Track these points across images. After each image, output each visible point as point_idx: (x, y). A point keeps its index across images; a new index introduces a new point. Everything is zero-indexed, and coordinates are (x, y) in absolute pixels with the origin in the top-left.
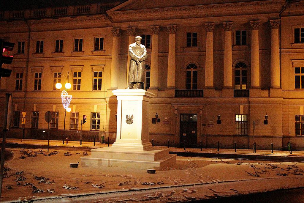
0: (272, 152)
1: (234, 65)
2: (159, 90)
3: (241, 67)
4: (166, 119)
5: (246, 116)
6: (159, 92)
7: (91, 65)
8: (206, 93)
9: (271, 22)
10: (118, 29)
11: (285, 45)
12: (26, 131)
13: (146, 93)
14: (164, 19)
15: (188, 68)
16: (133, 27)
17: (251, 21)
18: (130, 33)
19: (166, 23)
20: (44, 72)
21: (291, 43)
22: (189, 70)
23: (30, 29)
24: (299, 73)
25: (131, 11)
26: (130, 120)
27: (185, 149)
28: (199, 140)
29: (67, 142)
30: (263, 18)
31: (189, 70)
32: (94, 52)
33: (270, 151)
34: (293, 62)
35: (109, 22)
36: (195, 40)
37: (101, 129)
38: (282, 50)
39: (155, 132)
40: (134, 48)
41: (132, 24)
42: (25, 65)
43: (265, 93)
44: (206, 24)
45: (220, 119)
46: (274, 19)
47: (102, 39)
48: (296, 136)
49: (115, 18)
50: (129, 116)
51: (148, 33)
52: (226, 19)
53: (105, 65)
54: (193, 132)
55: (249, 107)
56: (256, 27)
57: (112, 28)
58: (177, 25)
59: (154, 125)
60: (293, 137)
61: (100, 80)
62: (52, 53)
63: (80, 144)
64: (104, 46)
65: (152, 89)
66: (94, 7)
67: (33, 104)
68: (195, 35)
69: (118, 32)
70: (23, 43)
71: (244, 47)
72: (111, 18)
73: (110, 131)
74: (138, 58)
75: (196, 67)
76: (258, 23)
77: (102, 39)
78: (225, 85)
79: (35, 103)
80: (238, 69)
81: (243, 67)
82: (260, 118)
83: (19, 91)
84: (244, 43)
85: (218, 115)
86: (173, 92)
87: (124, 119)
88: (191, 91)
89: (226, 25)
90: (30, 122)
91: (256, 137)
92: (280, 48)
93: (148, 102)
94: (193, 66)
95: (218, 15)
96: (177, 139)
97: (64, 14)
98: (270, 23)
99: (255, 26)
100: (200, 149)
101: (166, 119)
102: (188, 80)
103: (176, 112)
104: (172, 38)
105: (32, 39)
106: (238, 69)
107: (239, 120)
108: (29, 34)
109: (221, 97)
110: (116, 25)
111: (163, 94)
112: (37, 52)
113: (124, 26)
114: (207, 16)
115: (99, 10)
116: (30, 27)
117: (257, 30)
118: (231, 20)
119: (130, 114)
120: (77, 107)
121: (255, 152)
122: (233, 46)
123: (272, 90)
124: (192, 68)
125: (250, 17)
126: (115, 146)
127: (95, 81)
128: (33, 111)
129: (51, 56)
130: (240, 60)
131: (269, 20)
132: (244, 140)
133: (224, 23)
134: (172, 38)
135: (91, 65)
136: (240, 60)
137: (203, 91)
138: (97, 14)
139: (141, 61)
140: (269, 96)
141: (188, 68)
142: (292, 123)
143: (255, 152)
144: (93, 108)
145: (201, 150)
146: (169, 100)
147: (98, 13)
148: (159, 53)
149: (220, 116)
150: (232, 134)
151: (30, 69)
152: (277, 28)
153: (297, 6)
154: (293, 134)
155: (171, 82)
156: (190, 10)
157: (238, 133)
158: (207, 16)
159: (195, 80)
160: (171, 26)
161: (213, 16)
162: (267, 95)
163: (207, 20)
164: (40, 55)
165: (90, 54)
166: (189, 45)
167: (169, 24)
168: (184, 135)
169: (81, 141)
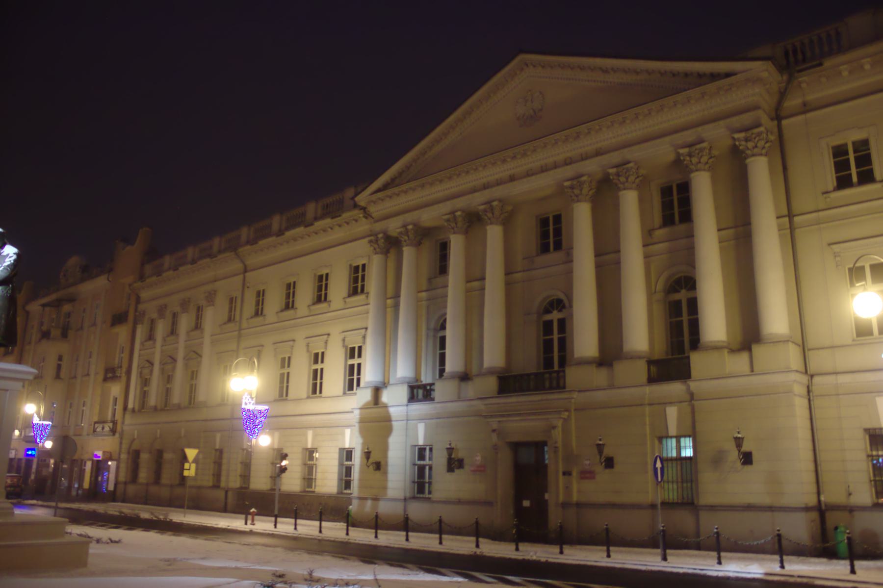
3: (555, 312)
8: (572, 375)
12: (230, 494)
19: (477, 201)
22: (548, 317)
28: (555, 517)
29: (253, 520)
31: (548, 317)
41: (409, 217)
43: (741, 362)
46: (746, 130)
49: (372, 209)
52: (615, 157)
53: (329, 335)
60: (863, 508)
63: (273, 527)
70: (236, 297)
79: (671, 403)
80: (676, 297)
83: (284, 400)
86: (492, 383)
88: (556, 372)
91: (712, 508)
95: (598, 153)
97: (264, 233)
104: (494, 234)
106: (676, 297)
109: (612, 386)
110: (378, 226)
111: (471, 389)
113: (394, 226)
114: (568, 162)
117: (703, 173)
120: (315, 436)
132: (684, 520)
134: (630, 201)
135: (343, 332)
140: (752, 371)
141: (547, 311)
145: (517, 549)
148: (778, 218)
149: (603, 445)
156: (524, 155)
157: (671, 497)
158: (568, 162)
159: (563, 343)
161: (584, 158)
162: (746, 369)
163: (569, 171)
168: (526, 503)
169: (276, 517)
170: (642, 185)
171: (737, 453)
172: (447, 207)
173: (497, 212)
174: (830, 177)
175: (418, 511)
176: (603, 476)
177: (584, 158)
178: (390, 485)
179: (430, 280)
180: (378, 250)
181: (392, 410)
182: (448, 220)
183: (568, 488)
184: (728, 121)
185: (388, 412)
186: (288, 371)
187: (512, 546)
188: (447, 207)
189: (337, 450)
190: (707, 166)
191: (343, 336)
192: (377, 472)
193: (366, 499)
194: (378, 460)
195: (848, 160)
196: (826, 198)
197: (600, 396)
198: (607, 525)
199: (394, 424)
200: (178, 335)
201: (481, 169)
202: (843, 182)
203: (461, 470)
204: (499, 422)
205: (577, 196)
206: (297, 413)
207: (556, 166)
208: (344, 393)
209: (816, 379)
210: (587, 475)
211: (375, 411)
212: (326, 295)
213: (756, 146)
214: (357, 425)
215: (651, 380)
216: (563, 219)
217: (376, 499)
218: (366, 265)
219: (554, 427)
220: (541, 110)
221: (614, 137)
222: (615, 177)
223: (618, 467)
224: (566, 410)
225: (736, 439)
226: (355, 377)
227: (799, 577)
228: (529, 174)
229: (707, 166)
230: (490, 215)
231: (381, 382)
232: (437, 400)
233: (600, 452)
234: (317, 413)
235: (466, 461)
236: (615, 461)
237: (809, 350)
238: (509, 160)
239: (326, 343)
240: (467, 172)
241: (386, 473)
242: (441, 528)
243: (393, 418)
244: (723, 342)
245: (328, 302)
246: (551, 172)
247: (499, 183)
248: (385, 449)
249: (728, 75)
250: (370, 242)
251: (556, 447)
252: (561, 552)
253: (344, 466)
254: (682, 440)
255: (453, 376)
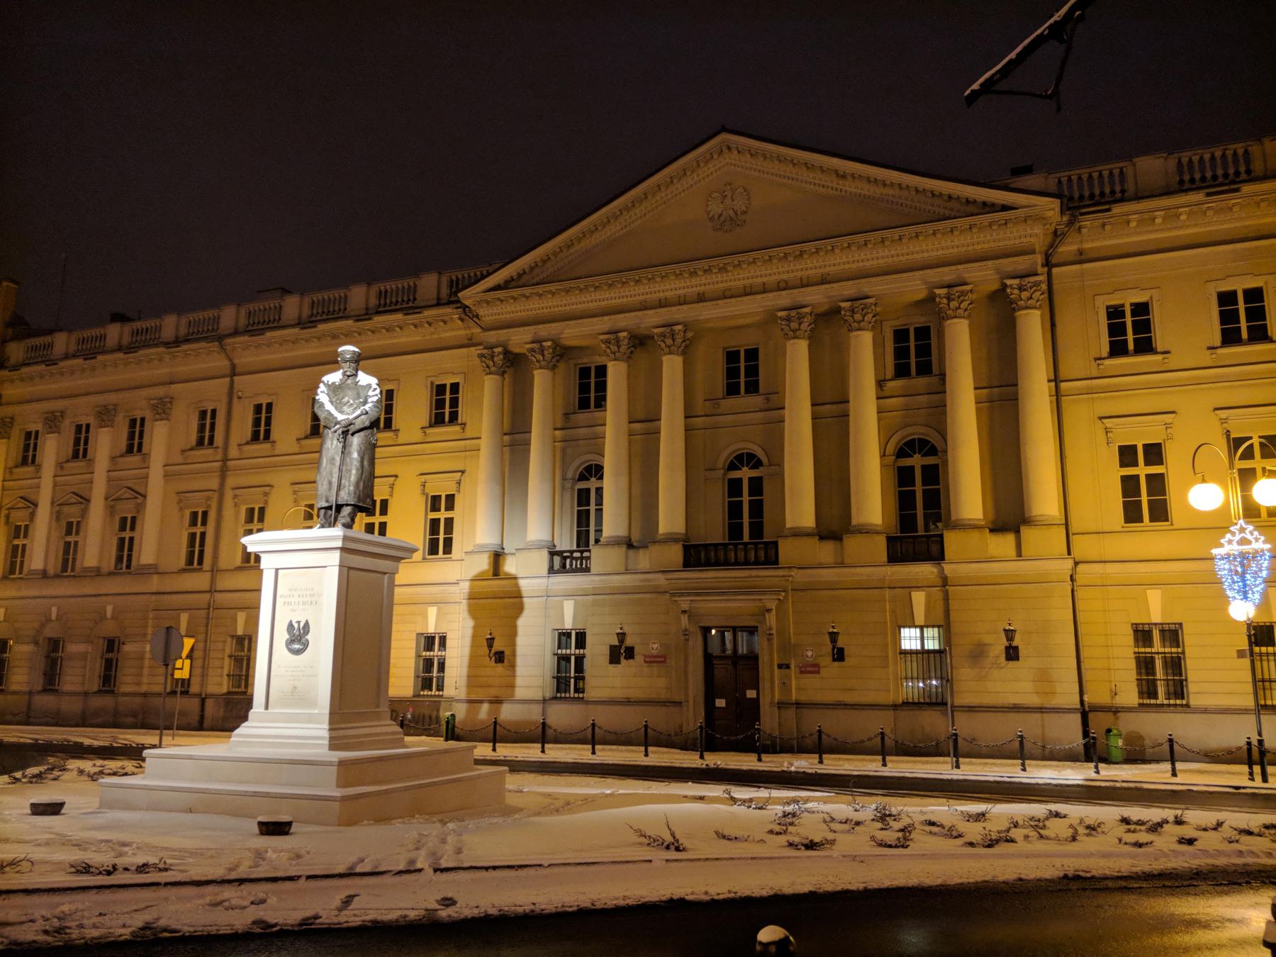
0: (1023, 765)
1: (891, 448)
2: (630, 545)
4: (655, 646)
5: (941, 629)
6: (631, 552)
7: (421, 474)
8: (787, 550)
9: (1011, 286)
10: (500, 349)
11: (1073, 363)
13: (345, 538)
14: (644, 307)
15: (732, 467)
16: (546, 341)
17: (938, 291)
18: (538, 361)
19: (650, 320)
20: (270, 501)
21: (1096, 359)
22: (735, 475)
23: (233, 366)
24: (1135, 464)
25: (540, 289)
26: (298, 638)
27: (702, 757)
28: (769, 722)
30: (984, 277)
31: (735, 475)
32: (429, 431)
33: (1014, 765)
34: (1108, 426)
35: (477, 330)
36: (753, 371)
37: (449, 691)
38: (1063, 385)
39: (618, 694)
40: (334, 389)
41: (543, 330)
42: (214, 484)
43: (1003, 544)
44: (780, 314)
45: (840, 644)
46: (1021, 277)
47: (455, 387)
48: (1141, 705)
49: (485, 312)
50: (296, 625)
51: (600, 360)
52: (849, 289)
53: (463, 472)
54: (751, 694)
55: (946, 598)
56: (959, 308)
57: (481, 347)
58: (687, 326)
59: (613, 669)
60: (1129, 710)
61: (449, 522)
62: (298, 440)
64: (460, 409)
65: (607, 544)
66: (428, 284)
67: (234, 611)
68: (752, 354)
69: (499, 359)
70: (214, 412)
71: (921, 382)
72: (477, 316)
73: (474, 697)
74: (339, 419)
75: (757, 464)
76: (963, 294)
77: (455, 387)
78: (854, 522)
80: (907, 462)
81: (925, 455)
82: (988, 639)
84: (925, 369)
85: (831, 630)
86: (675, 554)
87: (282, 636)
88: (746, 544)
89: (853, 311)
90: (226, 672)
91: (971, 709)
92: (1056, 379)
93: (386, 573)
94: (751, 460)
95: (824, 280)
96: (692, 718)
98: (1008, 291)
99: (954, 304)
100: (754, 757)
101: (655, 647)
102: (734, 510)
103: (684, 620)
104: (672, 367)
105: (239, 398)
107: (914, 647)
108: (232, 382)
109: (841, 564)
110: (492, 337)
111: (643, 559)
112: (255, 438)
113: (519, 340)
115: (445, 291)
116: (236, 361)
117: (962, 320)
118: (870, 294)
119: (299, 617)
121: (958, 767)
122: (880, 384)
123: (1025, 531)
124: (745, 469)
125: (935, 275)
126: (242, 736)
127: (434, 524)
128: (234, 634)
129: (296, 450)
130: (909, 430)
131: (1002, 278)
132: (933, 724)
133: (843, 305)
134: (672, 367)
135: (421, 474)
136: (909, 430)
137: (776, 544)
138: (439, 304)
139: (352, 429)
140: (1019, 554)
141: (732, 467)
142: (1125, 652)
143: (958, 767)
144: (425, 616)
146: (661, 580)
147: (442, 302)
149: (838, 633)
150: (890, 698)
151: (229, 494)
152: (1036, 308)
153: (1104, 225)
154: (1129, 695)
155: (670, 518)
156: (723, 269)
159: (757, 509)
160: (667, 330)
161: (805, 284)
162: (1012, 552)
163: (785, 298)
164: (263, 447)
165: (418, 436)
166: (732, 390)
167: (661, 323)
168: (720, 703)
170: (877, 327)
171: (831, 646)
172: (604, 324)
173: (679, 340)
174: (1214, 332)
175: (563, 716)
176: (831, 669)
177: (805, 284)
178: (519, 681)
179: (566, 415)
180: (493, 369)
181: (522, 583)
182: (607, 342)
183: (785, 685)
184: (998, 262)
185: (517, 585)
186: (202, 530)
187: (696, 756)
188: (604, 324)
189: (414, 637)
190: (870, 325)
191: (423, 480)
192: (500, 665)
193: (481, 702)
194: (501, 649)
195: (596, 378)
196: (1099, 365)
197: (827, 575)
198: (819, 727)
199: (525, 600)
200: (91, 461)
201: (645, 281)
202: (1118, 349)
203: (631, 661)
204: (692, 601)
205: (794, 331)
206: (177, 590)
207: (764, 290)
208: (424, 558)
209: (1081, 567)
210: (812, 669)
211: (496, 585)
212: (34, 456)
213: (1031, 298)
214: (465, 602)
215: (893, 558)
216: (274, 407)
217: (497, 701)
218: (395, 392)
219: (769, 610)
220: (745, 213)
221: (848, 263)
222: (848, 313)
223: (849, 661)
224: (784, 591)
225: (831, 634)
226: (442, 537)
227: (1123, 781)
228: (726, 295)
229: (870, 325)
230: (669, 341)
231: (625, 537)
232: (593, 570)
233: (490, 646)
234: (249, 588)
235: (636, 650)
236: (846, 653)
237: (1073, 534)
238: (700, 273)
239: (459, 483)
240: (637, 282)
241: (513, 666)
242: (593, 738)
243: (524, 594)
244: (877, 525)
245: (90, 460)
246: (758, 297)
247: (682, 301)
248: (512, 634)
249: (1005, 208)
250: (481, 356)
251: (770, 634)
252: (821, 762)
253: (422, 658)
254: (925, 630)
255: (616, 542)
